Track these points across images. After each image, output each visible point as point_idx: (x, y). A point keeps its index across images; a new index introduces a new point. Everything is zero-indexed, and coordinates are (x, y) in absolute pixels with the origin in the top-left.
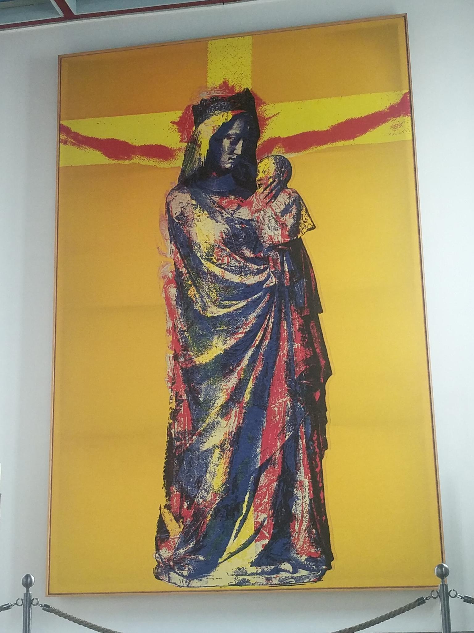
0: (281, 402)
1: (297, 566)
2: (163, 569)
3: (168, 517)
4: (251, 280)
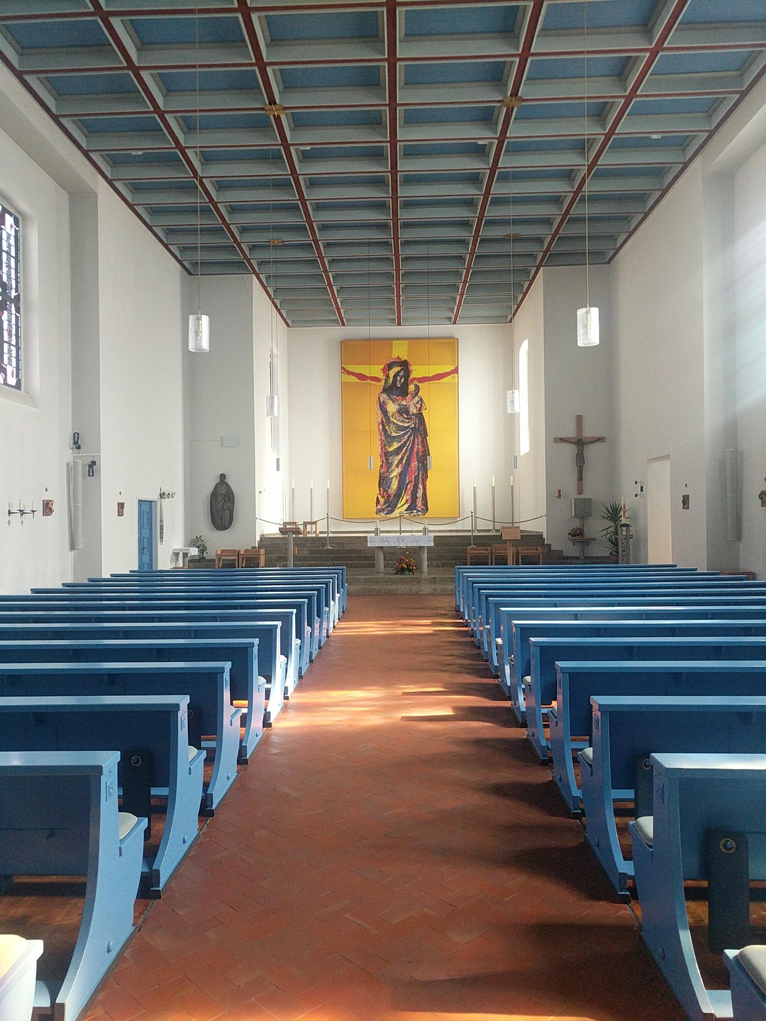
0: (415, 464)
1: (418, 511)
2: (378, 512)
3: (380, 497)
4: (406, 425)
